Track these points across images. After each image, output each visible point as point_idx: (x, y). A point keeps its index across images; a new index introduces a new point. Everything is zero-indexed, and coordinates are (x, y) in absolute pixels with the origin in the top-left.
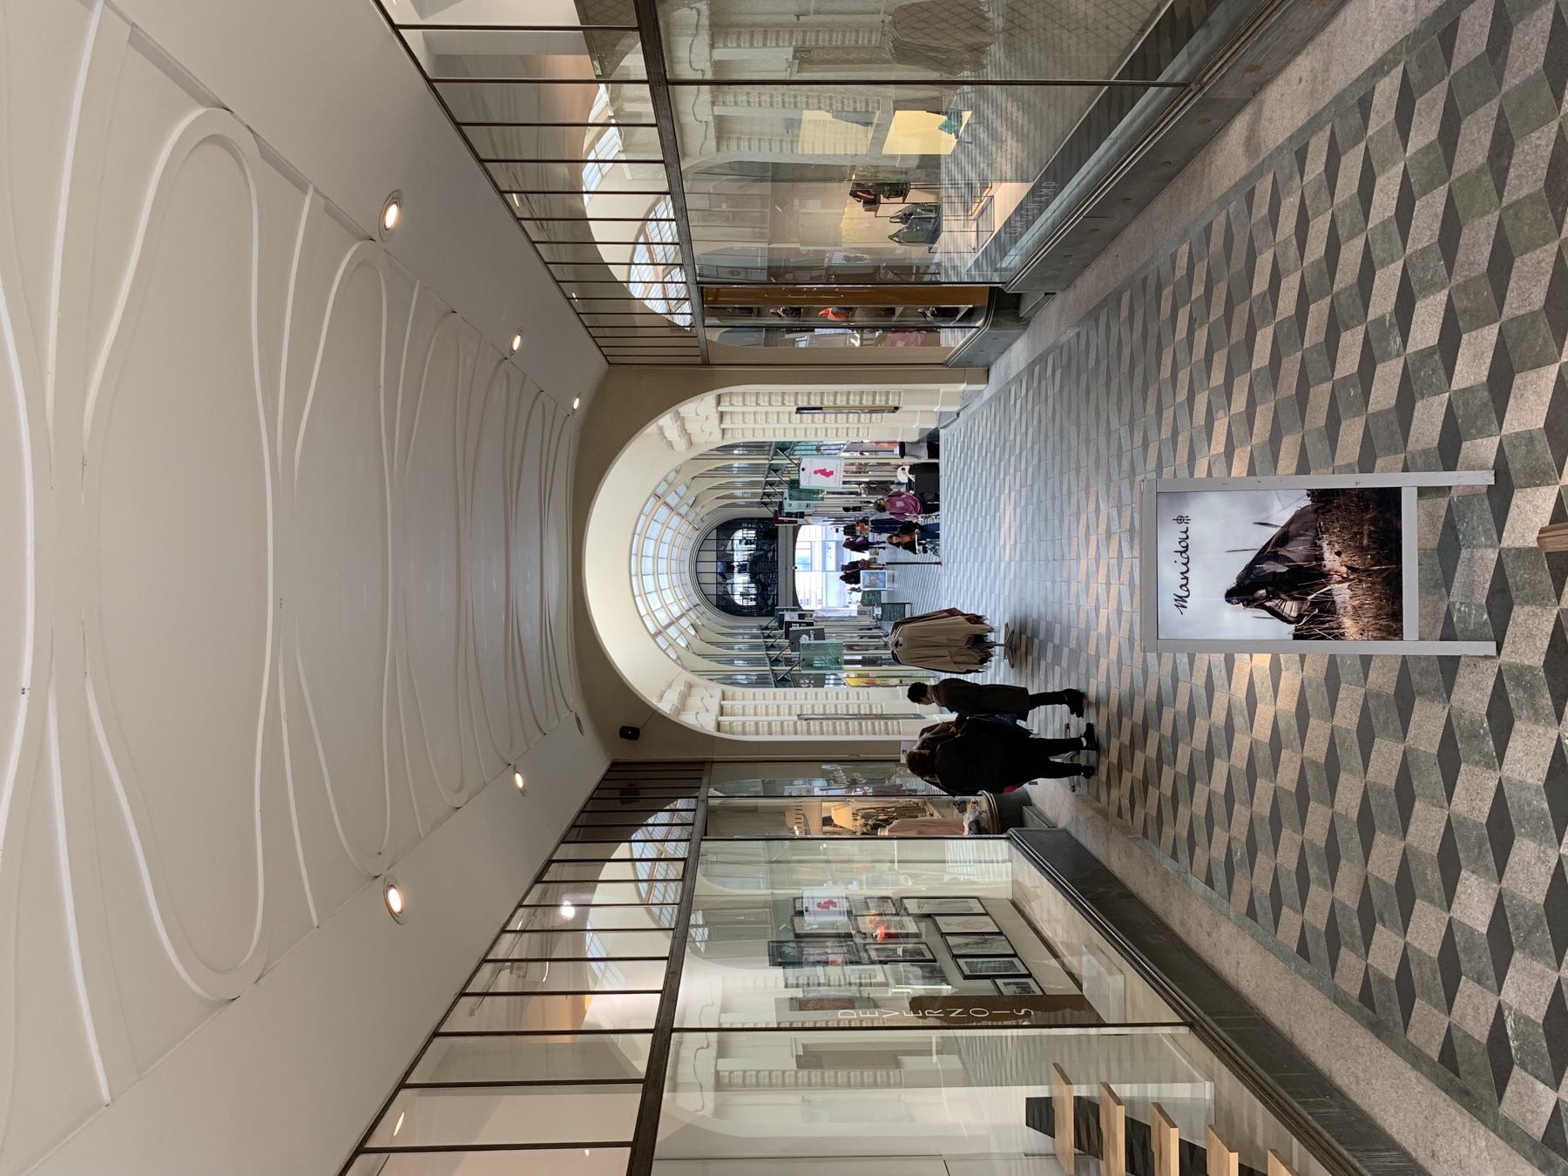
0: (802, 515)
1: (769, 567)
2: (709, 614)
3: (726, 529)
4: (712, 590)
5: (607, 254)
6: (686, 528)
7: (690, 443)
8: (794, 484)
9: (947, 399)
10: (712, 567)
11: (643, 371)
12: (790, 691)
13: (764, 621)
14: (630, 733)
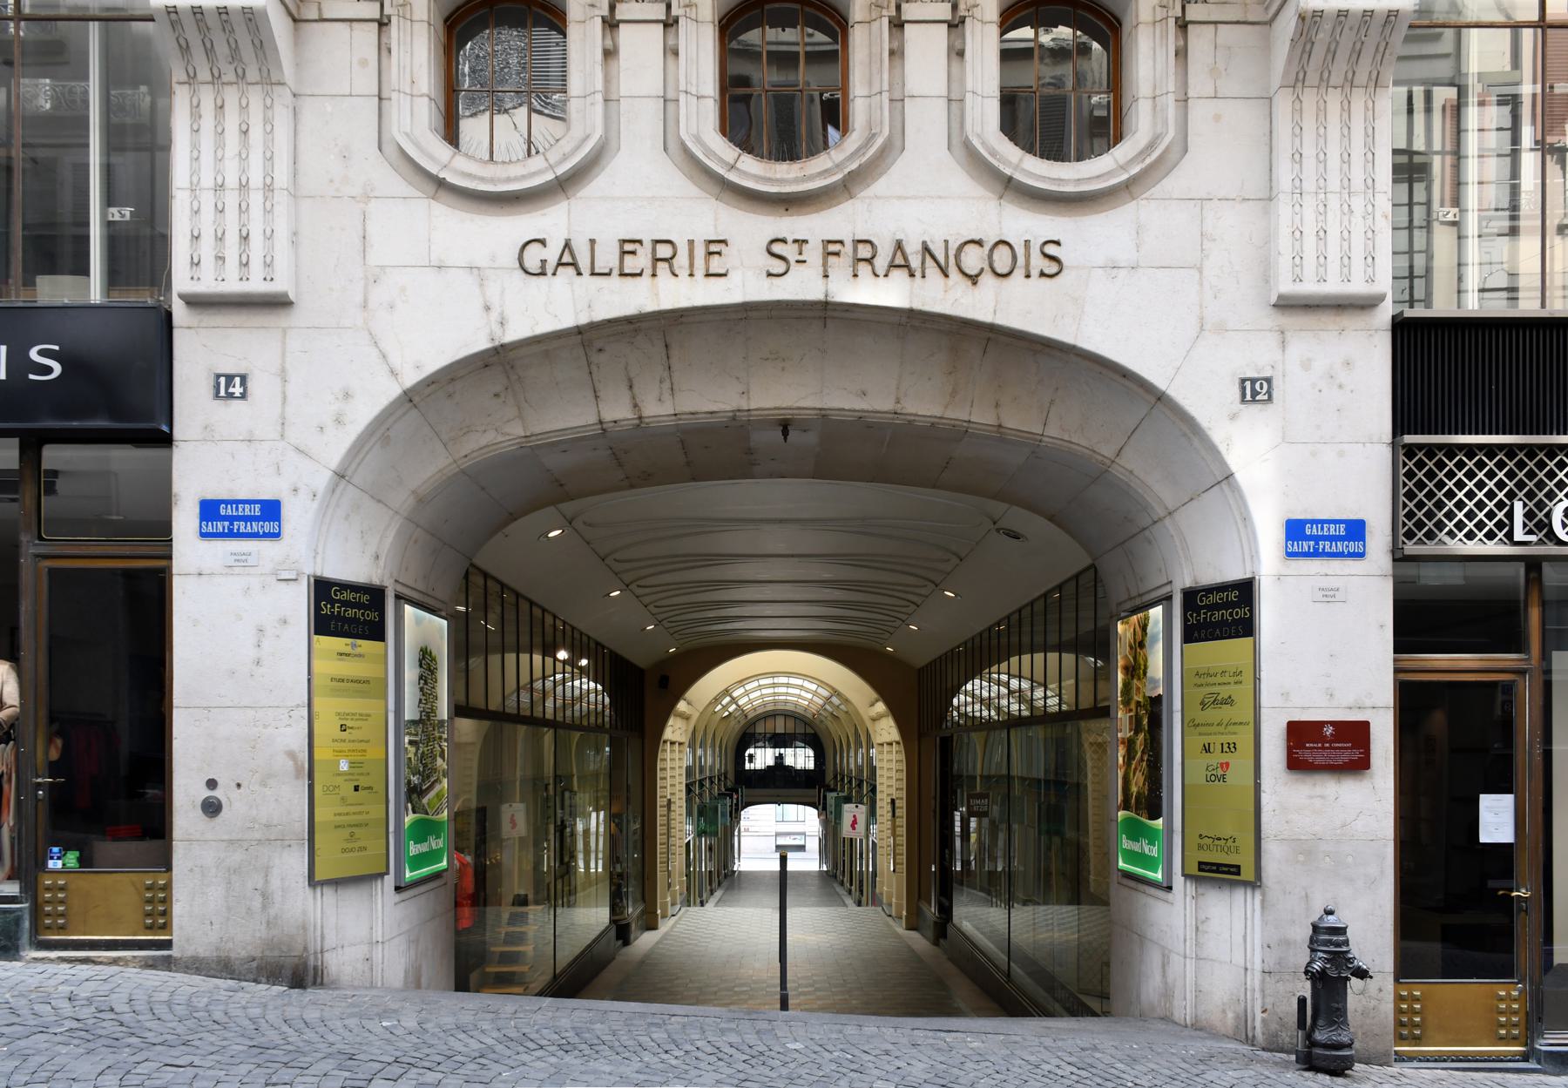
0: (824, 808)
1: (780, 785)
2: (738, 727)
3: (813, 739)
4: (760, 729)
5: (1014, 660)
6: (814, 709)
7: (874, 720)
8: (848, 800)
9: (899, 906)
10: (780, 730)
11: (918, 694)
12: (879, 788)
13: (731, 776)
14: (664, 682)
